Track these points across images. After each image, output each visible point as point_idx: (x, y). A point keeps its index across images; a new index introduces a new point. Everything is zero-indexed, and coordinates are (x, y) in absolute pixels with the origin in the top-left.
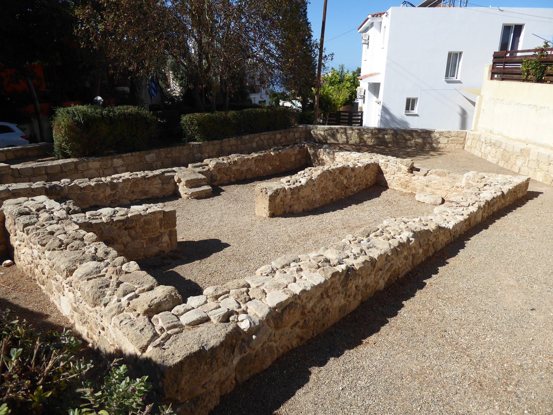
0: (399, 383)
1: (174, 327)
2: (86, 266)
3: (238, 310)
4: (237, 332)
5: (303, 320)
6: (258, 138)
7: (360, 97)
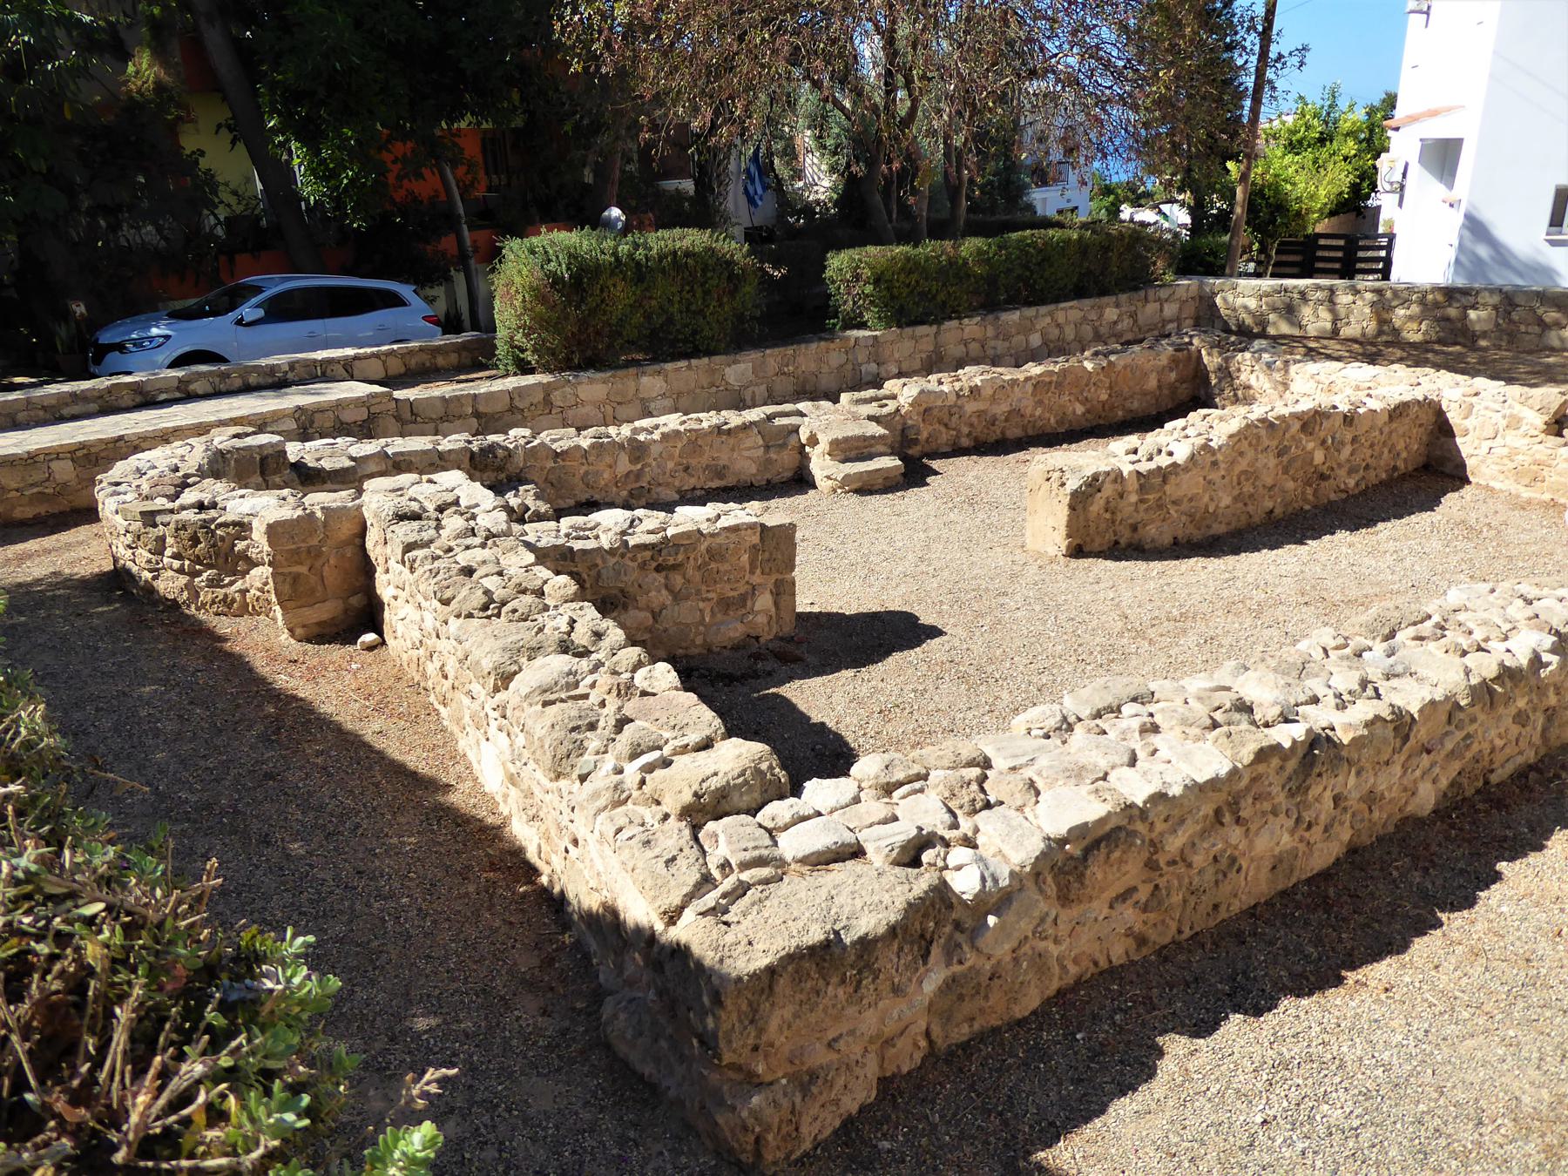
0: (1467, 1135)
1: (760, 862)
2: (543, 666)
3: (948, 835)
4: (942, 900)
5: (1150, 887)
6: (1048, 320)
7: (1388, 187)
